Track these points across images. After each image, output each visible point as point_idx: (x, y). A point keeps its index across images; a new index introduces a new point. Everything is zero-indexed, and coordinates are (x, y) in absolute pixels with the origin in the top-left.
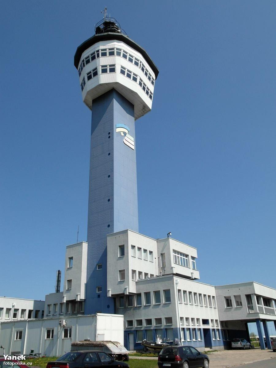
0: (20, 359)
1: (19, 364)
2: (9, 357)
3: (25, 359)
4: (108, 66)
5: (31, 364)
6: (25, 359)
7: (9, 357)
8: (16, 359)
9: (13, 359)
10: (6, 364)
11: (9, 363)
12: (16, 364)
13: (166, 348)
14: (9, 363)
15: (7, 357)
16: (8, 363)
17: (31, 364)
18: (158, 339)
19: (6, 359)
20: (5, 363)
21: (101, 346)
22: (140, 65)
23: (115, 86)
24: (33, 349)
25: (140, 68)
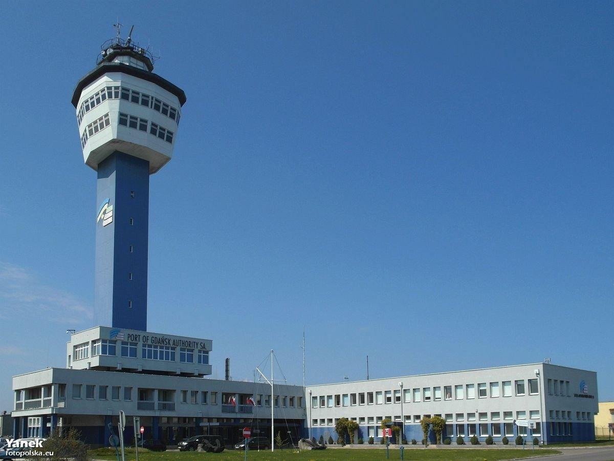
0: (34, 446)
1: (31, 454)
2: (14, 442)
3: (41, 446)
4: (113, 88)
5: (51, 453)
6: (41, 446)
7: (14, 442)
8: (26, 446)
9: (22, 446)
10: (11, 454)
11: (15, 453)
12: (27, 454)
13: (279, 438)
14: (15, 453)
15: (12, 444)
16: (14, 452)
17: (51, 453)
18: (241, 422)
19: (9, 446)
20: (28, 442)
21: (260, 434)
22: (152, 102)
23: (117, 147)
24: (91, 384)
25: (151, 107)
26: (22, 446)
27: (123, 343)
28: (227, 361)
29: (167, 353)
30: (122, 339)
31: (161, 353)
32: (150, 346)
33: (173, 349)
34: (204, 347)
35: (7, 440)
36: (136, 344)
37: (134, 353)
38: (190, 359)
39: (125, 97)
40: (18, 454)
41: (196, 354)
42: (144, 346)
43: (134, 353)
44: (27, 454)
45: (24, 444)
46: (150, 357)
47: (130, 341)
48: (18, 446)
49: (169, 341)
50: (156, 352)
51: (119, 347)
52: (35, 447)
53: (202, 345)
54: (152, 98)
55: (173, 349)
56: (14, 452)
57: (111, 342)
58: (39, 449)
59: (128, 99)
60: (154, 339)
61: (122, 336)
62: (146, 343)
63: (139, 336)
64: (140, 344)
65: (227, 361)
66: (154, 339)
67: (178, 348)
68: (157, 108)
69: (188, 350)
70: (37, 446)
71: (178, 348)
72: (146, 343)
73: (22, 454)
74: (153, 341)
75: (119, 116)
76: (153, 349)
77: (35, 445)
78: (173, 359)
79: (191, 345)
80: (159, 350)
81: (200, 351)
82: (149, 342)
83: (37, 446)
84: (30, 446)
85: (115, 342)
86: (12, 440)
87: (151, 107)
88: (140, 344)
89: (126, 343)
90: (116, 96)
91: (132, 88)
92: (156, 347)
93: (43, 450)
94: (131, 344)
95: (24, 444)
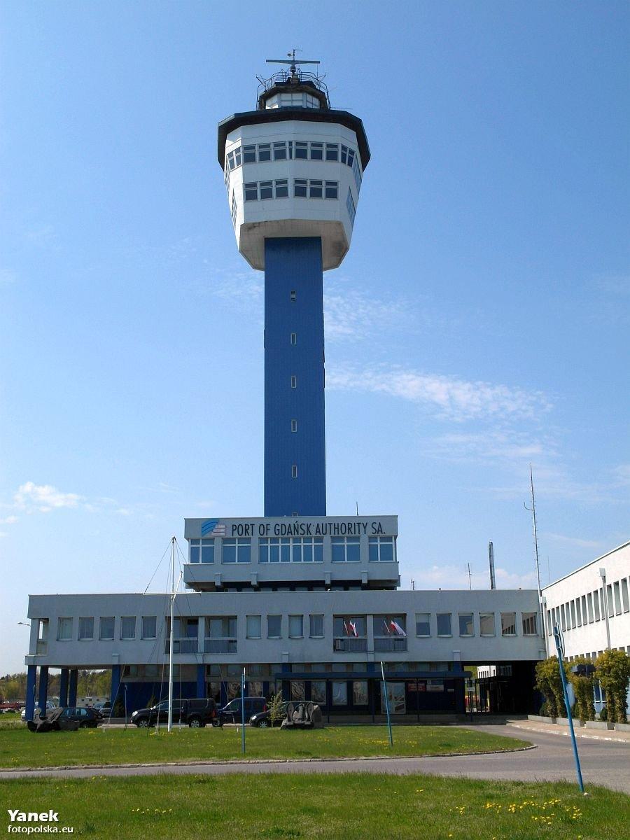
0: (46, 820)
2: (20, 814)
3: (56, 820)
5: (70, 830)
6: (56, 820)
7: (20, 814)
8: (36, 820)
9: (30, 820)
10: (15, 830)
12: (37, 830)
15: (17, 816)
16: (19, 828)
17: (70, 830)
22: (291, 150)
26: (30, 820)
27: (225, 540)
28: (319, 62)
29: (308, 549)
30: (222, 534)
31: (297, 549)
32: (274, 540)
33: (319, 540)
34: (380, 530)
35: (10, 811)
36: (249, 540)
37: (245, 555)
38: (354, 554)
39: (249, 158)
40: (24, 830)
41: (364, 544)
42: (263, 540)
43: (245, 555)
44: (37, 830)
45: (33, 817)
46: (275, 558)
47: (236, 535)
48: (24, 820)
49: (308, 528)
50: (286, 549)
51: (218, 547)
52: (48, 820)
53: (376, 526)
54: (291, 143)
55: (319, 540)
56: (19, 828)
57: (205, 541)
58: (53, 824)
59: (254, 160)
60: (280, 528)
61: (222, 530)
62: (265, 536)
63: (252, 525)
64: (255, 539)
65: (319, 62)
66: (280, 528)
67: (327, 538)
68: (301, 154)
69: (349, 539)
70: (51, 820)
71: (327, 538)
72: (265, 536)
73: (31, 830)
74: (276, 532)
75: (244, 189)
76: (280, 545)
77: (48, 818)
78: (319, 557)
79: (352, 530)
80: (291, 544)
81: (372, 539)
82: (271, 534)
83: (51, 820)
84: (41, 819)
85: (212, 540)
86: (17, 811)
87: (291, 157)
88: (255, 539)
89: (232, 540)
90: (238, 163)
91: (256, 141)
92: (287, 540)
93: (59, 824)
94: (241, 541)
95: (33, 817)
